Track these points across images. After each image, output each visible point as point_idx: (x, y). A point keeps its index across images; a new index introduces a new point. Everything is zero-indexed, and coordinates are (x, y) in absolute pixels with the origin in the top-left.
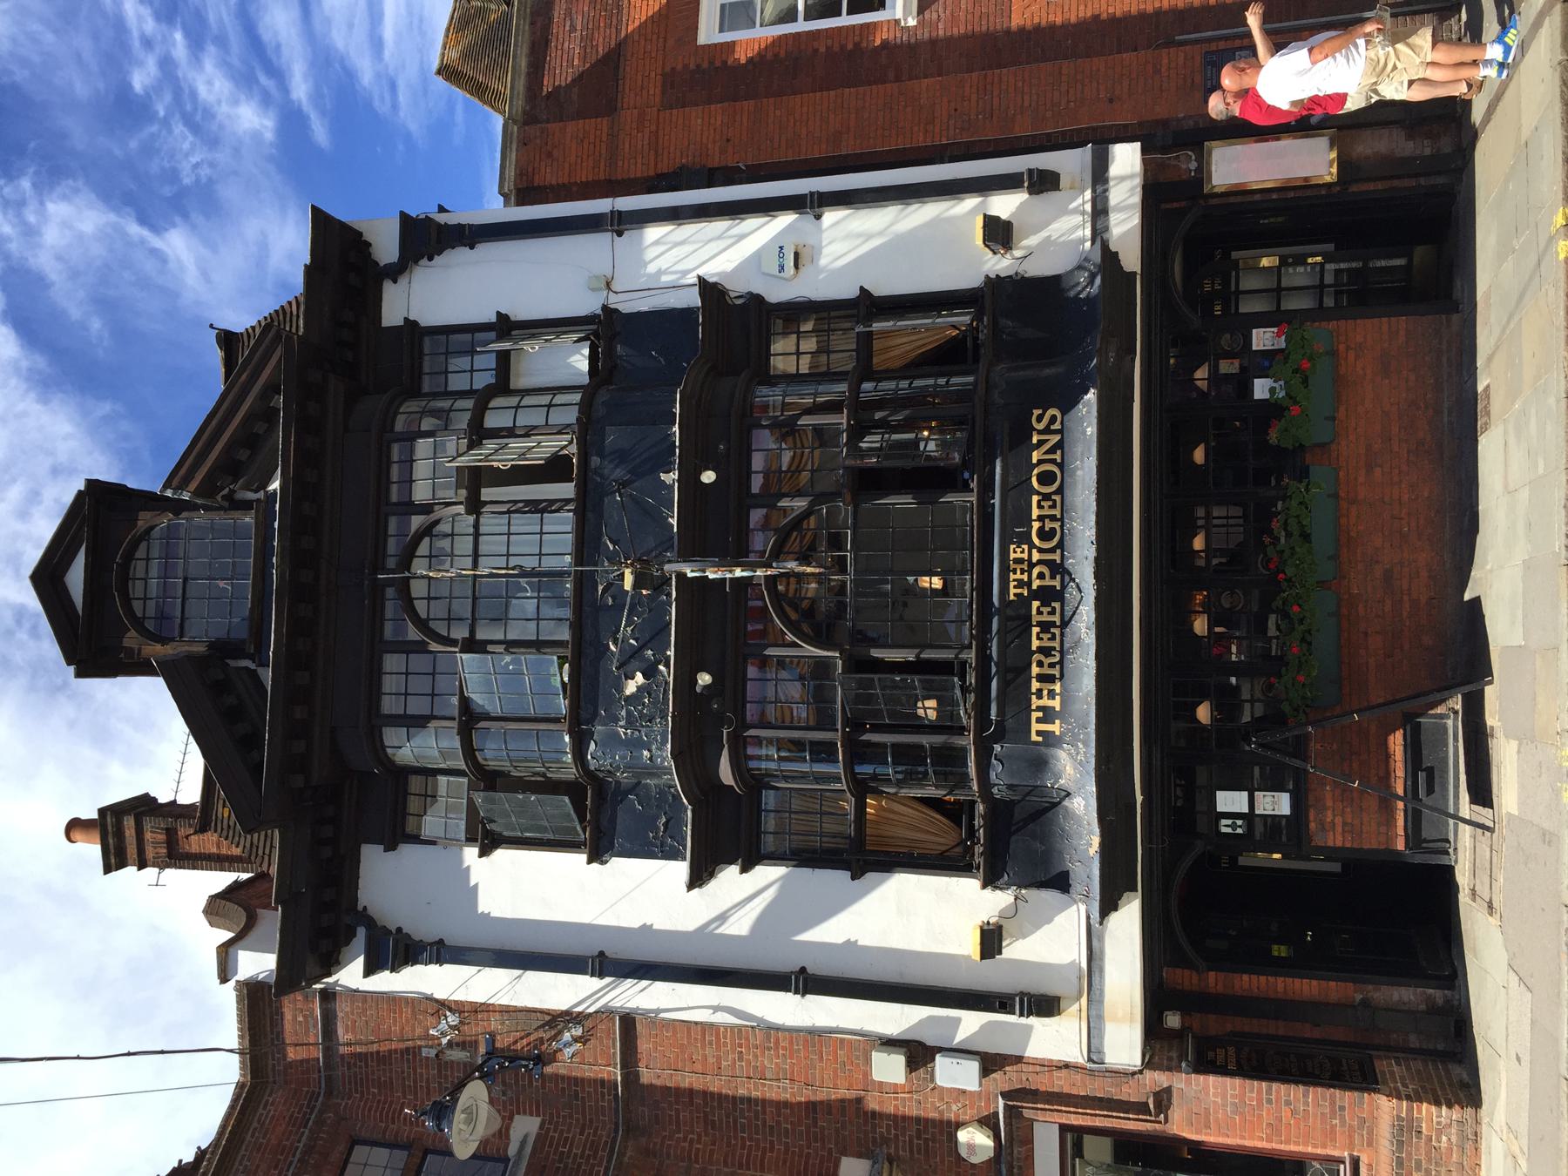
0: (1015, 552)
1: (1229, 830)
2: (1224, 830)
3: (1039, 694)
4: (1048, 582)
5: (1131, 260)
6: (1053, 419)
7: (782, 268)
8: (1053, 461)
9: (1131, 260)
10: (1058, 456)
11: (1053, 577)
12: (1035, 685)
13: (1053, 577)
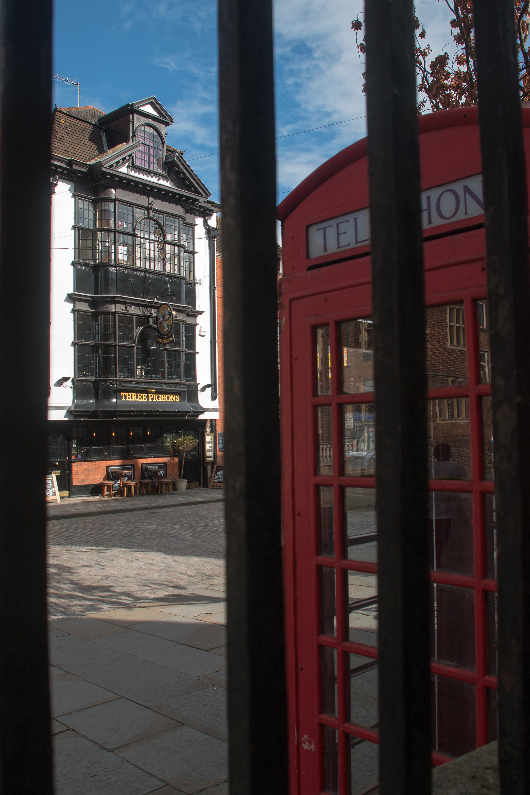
0: (145, 396)
1: (74, 443)
2: (74, 441)
3: (129, 395)
4: (150, 398)
5: (201, 417)
6: (178, 399)
7: (202, 332)
8: (155, 396)
9: (201, 417)
10: (172, 401)
11: (151, 399)
12: (130, 394)
13: (151, 399)
